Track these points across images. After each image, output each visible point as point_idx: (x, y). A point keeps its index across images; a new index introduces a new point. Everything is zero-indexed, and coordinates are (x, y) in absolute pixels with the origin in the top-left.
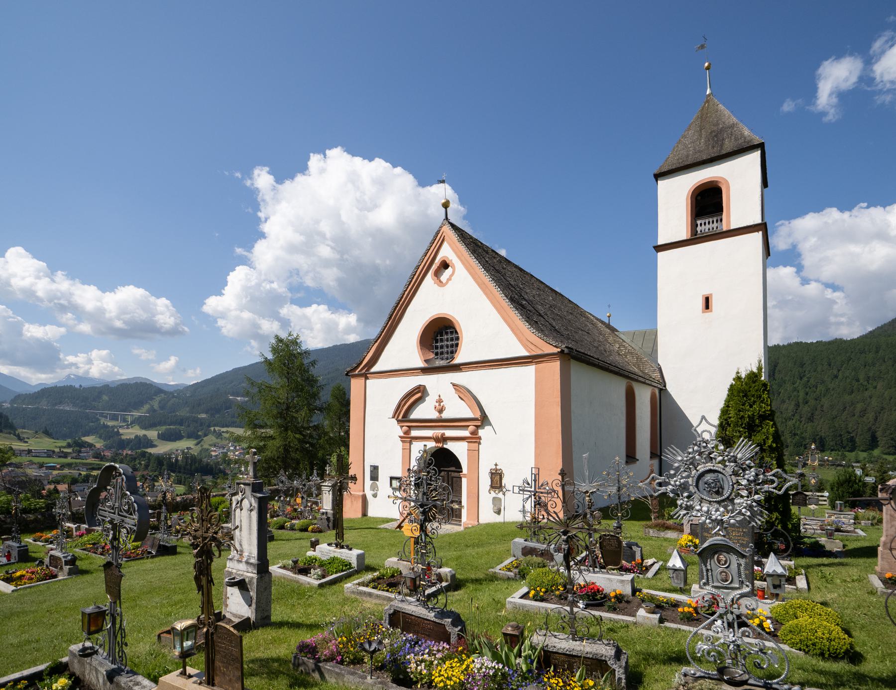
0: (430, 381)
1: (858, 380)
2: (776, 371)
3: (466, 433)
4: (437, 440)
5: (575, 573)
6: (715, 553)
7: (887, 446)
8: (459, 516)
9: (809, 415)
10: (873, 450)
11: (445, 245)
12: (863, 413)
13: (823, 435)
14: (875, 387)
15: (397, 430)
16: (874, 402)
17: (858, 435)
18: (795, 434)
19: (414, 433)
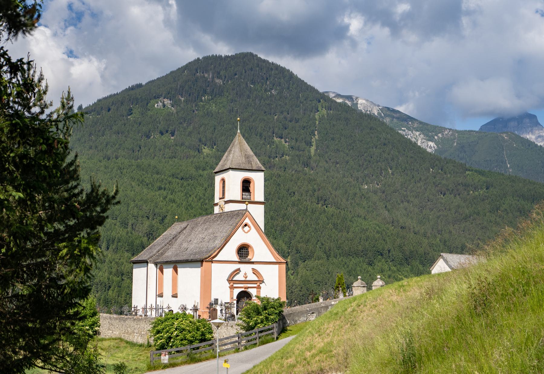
0: (243, 267)
3: (255, 285)
4: (245, 288)
5: (192, 314)
6: (367, 284)
11: (247, 218)
15: (228, 285)
19: (235, 285)
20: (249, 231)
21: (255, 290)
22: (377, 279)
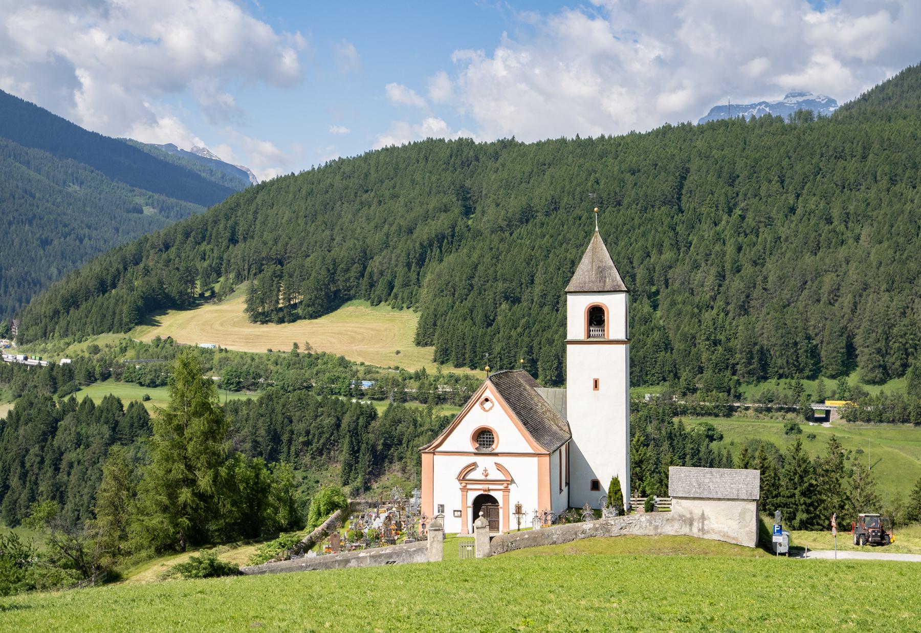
0: (479, 460)
1: (829, 221)
2: (684, 192)
3: (501, 487)
4: (485, 491)
7: (871, 366)
8: (498, 529)
9: (743, 297)
10: (848, 375)
11: (487, 390)
12: (835, 292)
13: (765, 342)
14: (857, 239)
15: (458, 485)
16: (853, 273)
17: (824, 344)
18: (716, 343)
19: (469, 487)
20: (491, 409)
21: (501, 493)
22: (479, 516)
